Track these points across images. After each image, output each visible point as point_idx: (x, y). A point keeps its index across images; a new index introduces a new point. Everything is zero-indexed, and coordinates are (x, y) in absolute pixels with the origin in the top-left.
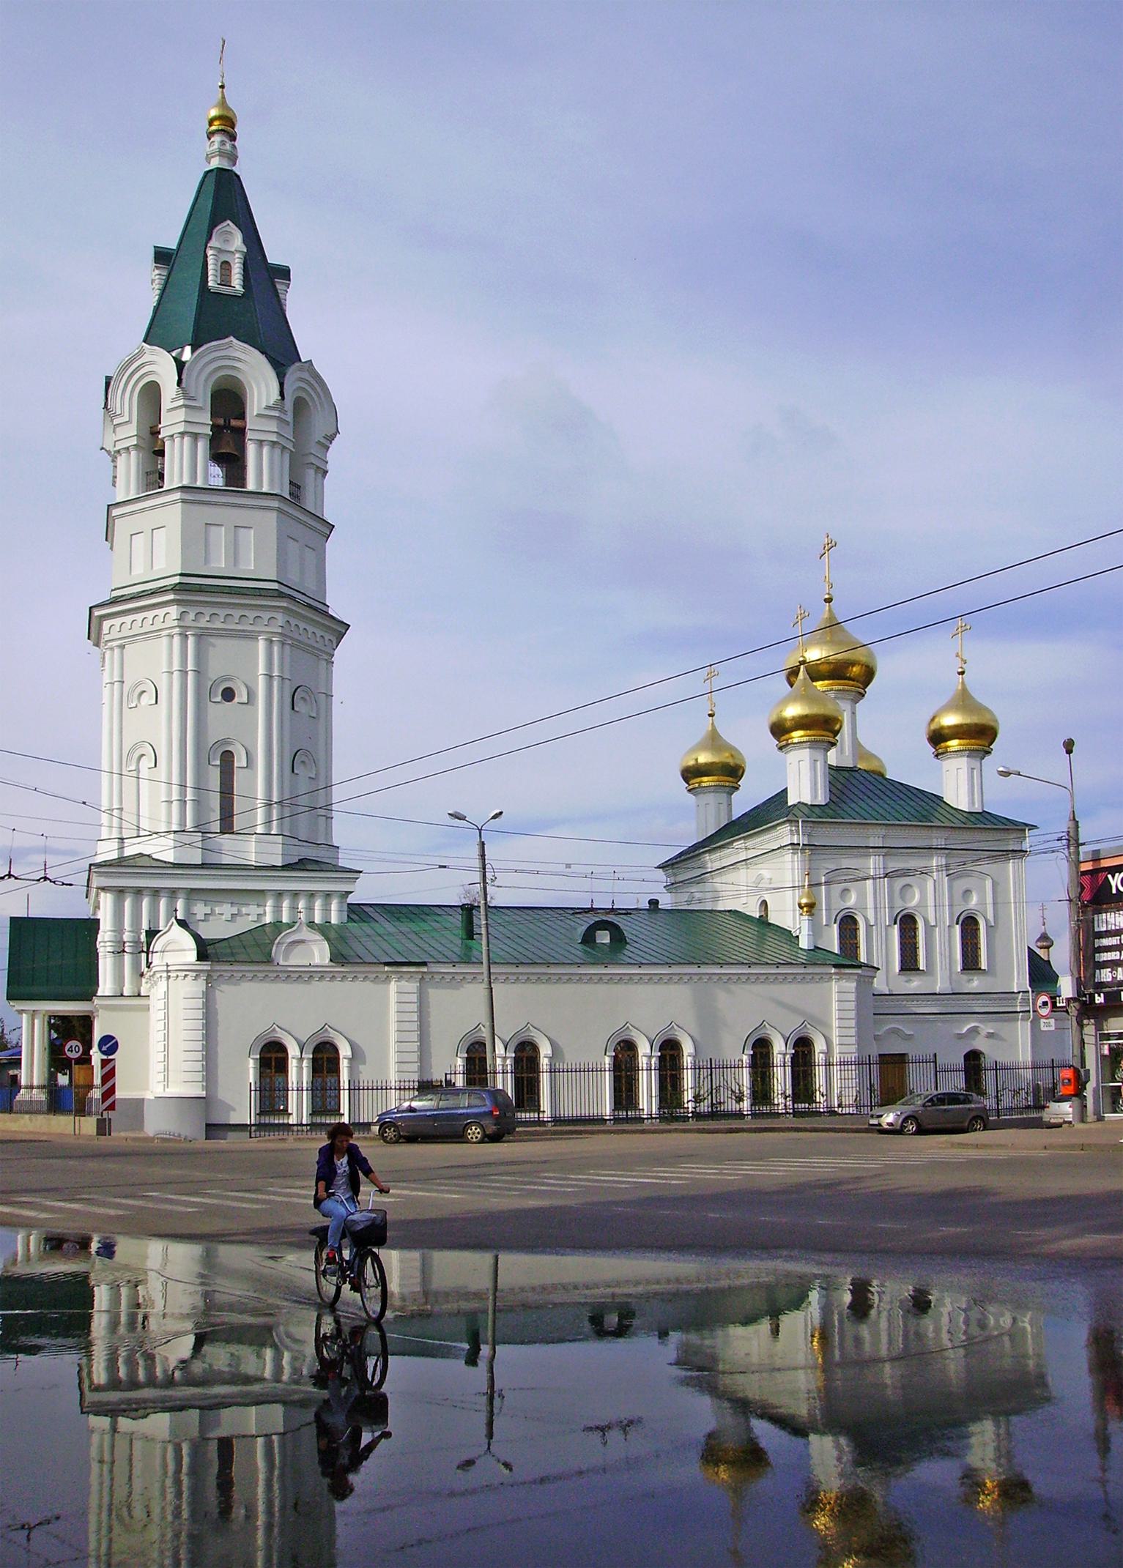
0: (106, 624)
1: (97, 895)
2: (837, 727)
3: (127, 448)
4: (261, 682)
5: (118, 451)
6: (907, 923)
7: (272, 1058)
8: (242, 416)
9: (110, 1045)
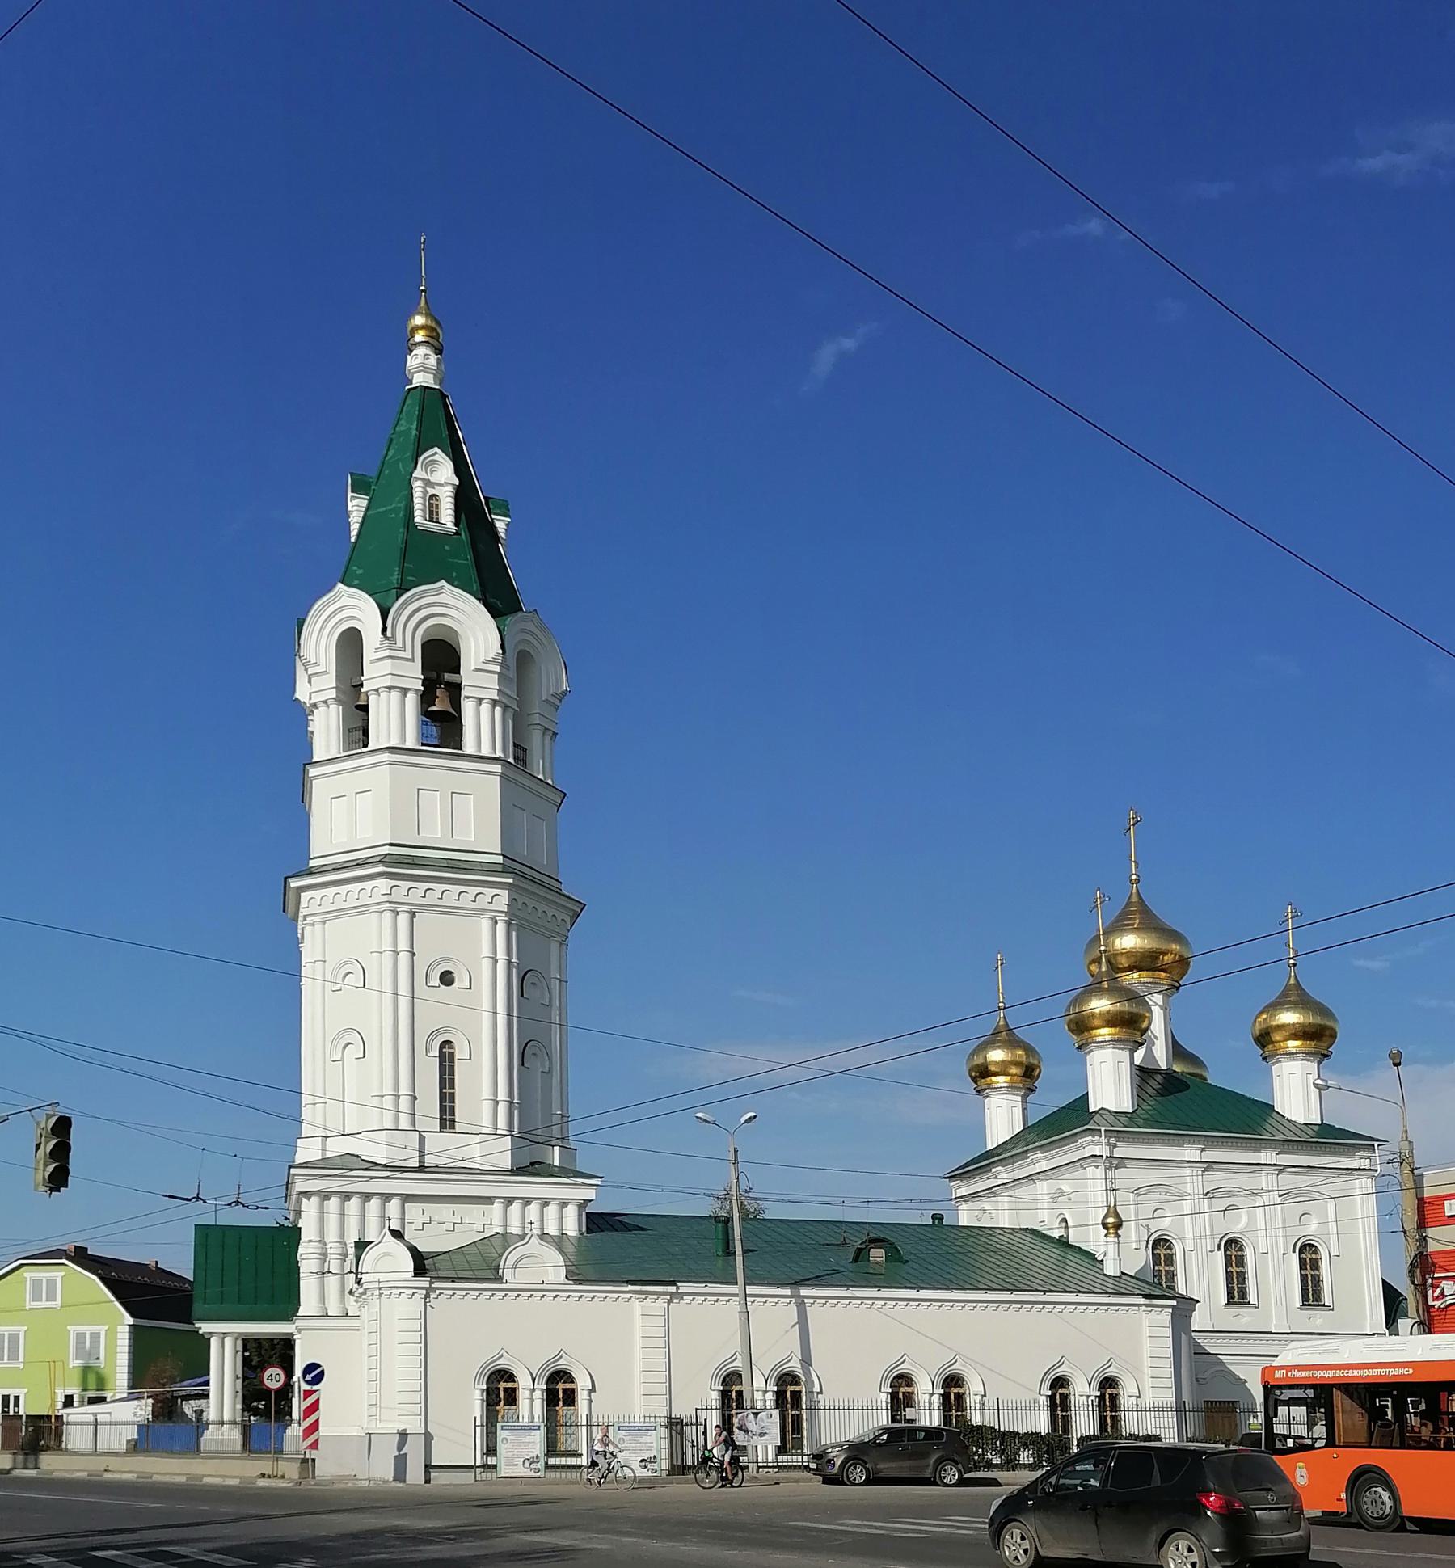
0: (305, 896)
1: (299, 1202)
2: (1144, 1025)
3: (325, 702)
4: (486, 964)
5: (315, 706)
6: (1233, 1248)
7: (499, 1389)
8: (456, 669)
9: (315, 1374)
